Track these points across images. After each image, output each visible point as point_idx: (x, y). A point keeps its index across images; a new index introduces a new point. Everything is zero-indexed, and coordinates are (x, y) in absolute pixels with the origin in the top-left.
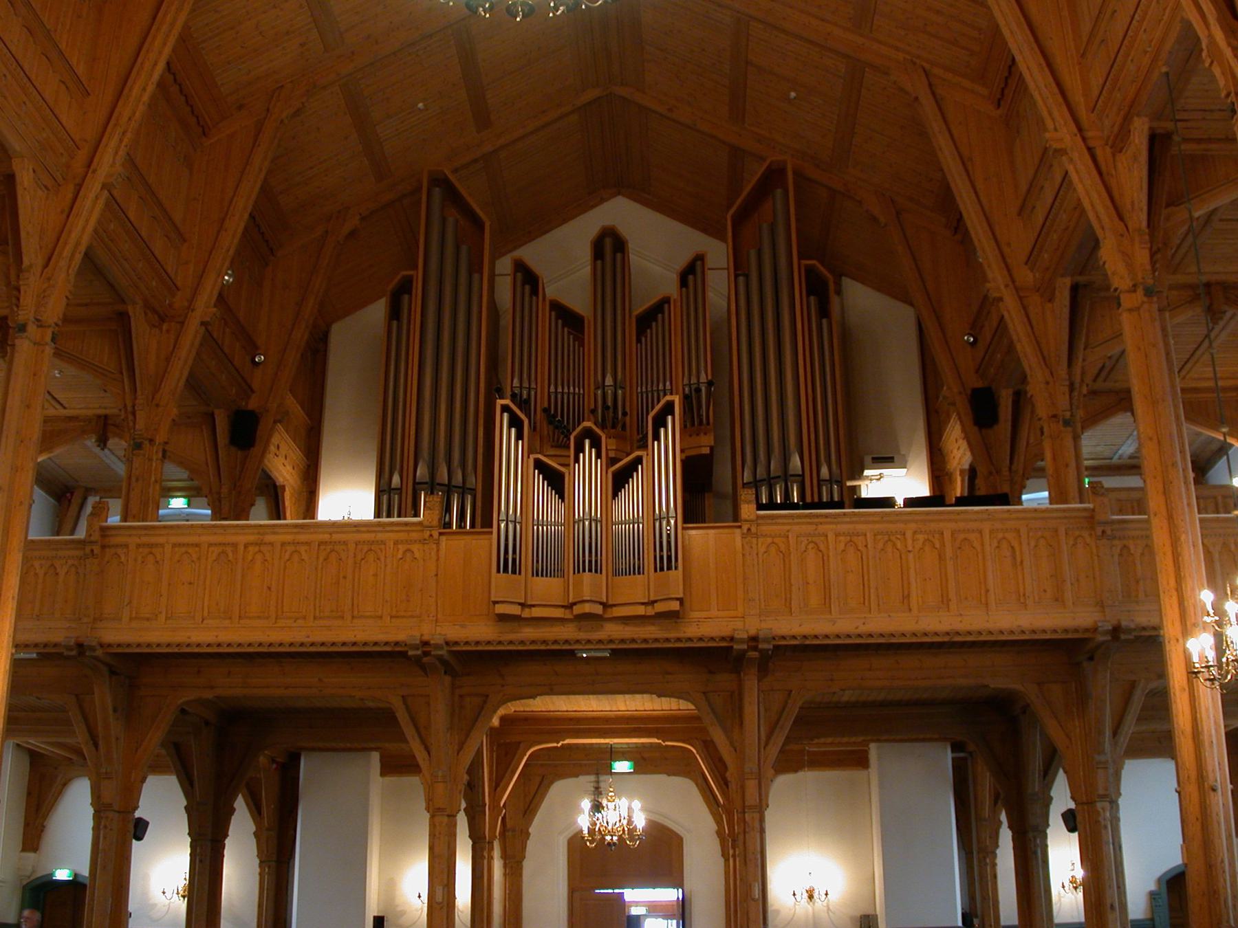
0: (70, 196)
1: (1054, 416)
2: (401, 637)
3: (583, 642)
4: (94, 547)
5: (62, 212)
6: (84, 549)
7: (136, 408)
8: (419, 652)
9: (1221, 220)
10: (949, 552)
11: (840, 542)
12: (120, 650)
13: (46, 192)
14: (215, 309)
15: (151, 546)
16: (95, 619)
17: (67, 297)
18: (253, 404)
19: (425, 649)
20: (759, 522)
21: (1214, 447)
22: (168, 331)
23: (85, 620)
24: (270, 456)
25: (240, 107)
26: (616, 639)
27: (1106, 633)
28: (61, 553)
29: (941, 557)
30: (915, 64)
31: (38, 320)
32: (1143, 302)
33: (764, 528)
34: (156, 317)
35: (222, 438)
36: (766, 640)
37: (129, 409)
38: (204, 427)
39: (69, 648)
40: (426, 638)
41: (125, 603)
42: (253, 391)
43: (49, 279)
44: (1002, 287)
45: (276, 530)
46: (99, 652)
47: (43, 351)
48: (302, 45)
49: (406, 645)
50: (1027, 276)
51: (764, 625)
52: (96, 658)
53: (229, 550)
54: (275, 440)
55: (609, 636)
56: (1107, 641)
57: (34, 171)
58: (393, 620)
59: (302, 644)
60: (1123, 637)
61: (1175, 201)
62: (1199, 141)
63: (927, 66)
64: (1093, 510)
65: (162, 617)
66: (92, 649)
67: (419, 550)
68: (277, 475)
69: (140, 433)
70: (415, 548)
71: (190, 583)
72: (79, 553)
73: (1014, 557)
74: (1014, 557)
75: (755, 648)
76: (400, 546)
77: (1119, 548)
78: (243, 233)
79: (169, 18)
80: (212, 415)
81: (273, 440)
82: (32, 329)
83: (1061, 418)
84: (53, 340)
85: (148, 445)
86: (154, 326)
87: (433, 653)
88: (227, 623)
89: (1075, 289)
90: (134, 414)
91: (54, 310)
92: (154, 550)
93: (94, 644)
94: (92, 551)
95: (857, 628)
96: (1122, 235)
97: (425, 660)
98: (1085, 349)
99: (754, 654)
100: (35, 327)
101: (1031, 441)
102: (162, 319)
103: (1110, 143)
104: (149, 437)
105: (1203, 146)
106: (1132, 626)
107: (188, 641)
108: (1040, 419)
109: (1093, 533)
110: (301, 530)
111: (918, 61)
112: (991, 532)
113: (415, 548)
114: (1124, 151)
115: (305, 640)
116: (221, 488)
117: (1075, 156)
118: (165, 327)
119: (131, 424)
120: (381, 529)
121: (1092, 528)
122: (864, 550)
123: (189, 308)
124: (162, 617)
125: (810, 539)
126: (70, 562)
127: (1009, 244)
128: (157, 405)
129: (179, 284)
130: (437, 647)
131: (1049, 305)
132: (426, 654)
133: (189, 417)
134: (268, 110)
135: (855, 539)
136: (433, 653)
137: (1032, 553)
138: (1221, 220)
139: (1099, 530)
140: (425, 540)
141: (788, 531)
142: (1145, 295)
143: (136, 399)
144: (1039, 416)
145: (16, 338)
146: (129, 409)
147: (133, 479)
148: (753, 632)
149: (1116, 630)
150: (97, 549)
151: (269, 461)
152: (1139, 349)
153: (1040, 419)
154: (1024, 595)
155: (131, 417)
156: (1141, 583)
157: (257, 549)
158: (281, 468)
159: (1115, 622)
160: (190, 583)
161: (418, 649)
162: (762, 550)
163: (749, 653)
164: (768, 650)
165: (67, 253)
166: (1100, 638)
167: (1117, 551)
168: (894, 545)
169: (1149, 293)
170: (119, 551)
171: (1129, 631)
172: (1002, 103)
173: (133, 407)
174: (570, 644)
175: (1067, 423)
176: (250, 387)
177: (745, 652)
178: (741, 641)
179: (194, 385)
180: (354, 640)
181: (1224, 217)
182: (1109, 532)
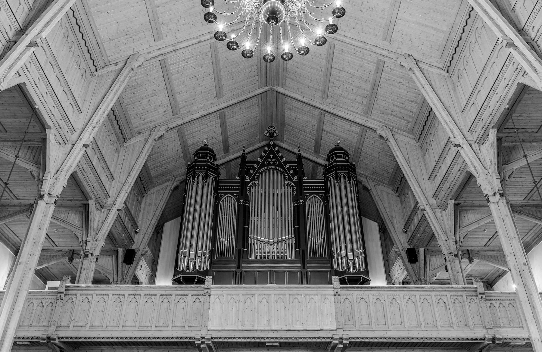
0: (69, 149)
1: (450, 253)
2: (192, 335)
3: (270, 339)
4: (61, 295)
5: (66, 154)
6: (57, 296)
7: (87, 241)
8: (200, 342)
9: (514, 177)
10: (419, 304)
11: (374, 298)
12: (67, 340)
13: (59, 145)
14: (124, 205)
15: (87, 295)
16: (57, 326)
17: (63, 186)
18: (134, 247)
19: (203, 341)
20: (341, 289)
21: (500, 272)
22: (104, 212)
23: (53, 326)
24: (138, 269)
25: (139, 133)
26: (288, 338)
27: (489, 340)
28: (46, 297)
29: (416, 306)
30: (386, 127)
31: (49, 194)
32: (499, 199)
33: (342, 292)
34: (99, 206)
35: (121, 260)
36: (346, 339)
37: (84, 241)
38: (113, 256)
39: (44, 339)
40: (203, 336)
41: (72, 319)
42: (134, 243)
43: (57, 178)
44: (425, 205)
45: (142, 289)
46: (57, 342)
47: (50, 207)
48: (165, 112)
49: (194, 339)
50: (433, 202)
51: (345, 333)
52: (55, 344)
53: (121, 297)
54: (141, 263)
55: (281, 336)
56: (490, 344)
57: (55, 135)
58: (189, 328)
59: (149, 338)
60: (497, 342)
61: (506, 163)
62: (512, 142)
63: (391, 128)
64: (477, 288)
65: (88, 326)
66: (54, 339)
67: (202, 298)
68: (140, 277)
69: (88, 250)
70: (200, 297)
71: (103, 311)
72: (55, 297)
73: (446, 306)
74: (446, 306)
75: (341, 343)
76: (194, 296)
77: (489, 304)
78: (135, 182)
79: (116, 88)
80: (117, 251)
81: (140, 263)
82: (46, 197)
83: (453, 254)
84: (55, 202)
85: (91, 256)
86: (99, 210)
87: (206, 342)
88: (117, 329)
89: (456, 206)
90: (86, 243)
91: (58, 190)
92: (88, 297)
93: (55, 337)
94: (61, 296)
95: (384, 335)
96: (487, 175)
97: (202, 346)
98: (459, 228)
99: (341, 346)
100: (48, 197)
101: (430, 269)
102: (102, 207)
103: (477, 142)
104: (91, 253)
105: (514, 143)
106: (501, 337)
107: (99, 336)
108: (444, 255)
109: (477, 297)
110: (153, 289)
111: (387, 126)
112: (435, 296)
113: (200, 297)
114: (484, 144)
115: (150, 336)
116: (118, 279)
117: (464, 146)
118: (103, 211)
119: (84, 247)
120: (187, 289)
121: (477, 296)
122: (384, 302)
123: (113, 204)
124: (88, 326)
125: (362, 297)
126: (50, 301)
127: (426, 190)
128: (96, 240)
129: (110, 195)
130: (208, 340)
131: (444, 212)
132: (203, 343)
133: (108, 252)
134: (150, 135)
135: (380, 298)
136: (206, 342)
137: (453, 305)
138: (514, 177)
139: (480, 296)
140: (205, 294)
141: (352, 294)
142: (500, 197)
143: (87, 237)
144: (444, 253)
145: (38, 200)
146: (84, 241)
147: (83, 269)
148: (341, 336)
149: (494, 339)
150: (63, 296)
151: (137, 271)
152: (500, 218)
153: (444, 255)
154: (452, 323)
155: (84, 245)
156: (501, 319)
157: (133, 296)
158: (142, 275)
159: (493, 336)
160: (103, 311)
161: (200, 341)
162: (342, 301)
163: (339, 345)
164: (347, 343)
165: (66, 168)
166: (487, 342)
167: (488, 305)
168: (396, 300)
169: (502, 195)
170: (73, 297)
171: (499, 339)
172: (419, 140)
173: (86, 240)
174: (264, 339)
175: (456, 256)
176: (133, 241)
177: (337, 344)
178: (336, 339)
179: (110, 237)
180: (172, 336)
181: (515, 176)
182: (484, 297)
